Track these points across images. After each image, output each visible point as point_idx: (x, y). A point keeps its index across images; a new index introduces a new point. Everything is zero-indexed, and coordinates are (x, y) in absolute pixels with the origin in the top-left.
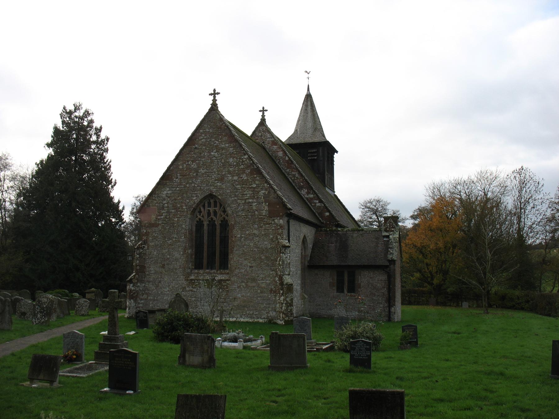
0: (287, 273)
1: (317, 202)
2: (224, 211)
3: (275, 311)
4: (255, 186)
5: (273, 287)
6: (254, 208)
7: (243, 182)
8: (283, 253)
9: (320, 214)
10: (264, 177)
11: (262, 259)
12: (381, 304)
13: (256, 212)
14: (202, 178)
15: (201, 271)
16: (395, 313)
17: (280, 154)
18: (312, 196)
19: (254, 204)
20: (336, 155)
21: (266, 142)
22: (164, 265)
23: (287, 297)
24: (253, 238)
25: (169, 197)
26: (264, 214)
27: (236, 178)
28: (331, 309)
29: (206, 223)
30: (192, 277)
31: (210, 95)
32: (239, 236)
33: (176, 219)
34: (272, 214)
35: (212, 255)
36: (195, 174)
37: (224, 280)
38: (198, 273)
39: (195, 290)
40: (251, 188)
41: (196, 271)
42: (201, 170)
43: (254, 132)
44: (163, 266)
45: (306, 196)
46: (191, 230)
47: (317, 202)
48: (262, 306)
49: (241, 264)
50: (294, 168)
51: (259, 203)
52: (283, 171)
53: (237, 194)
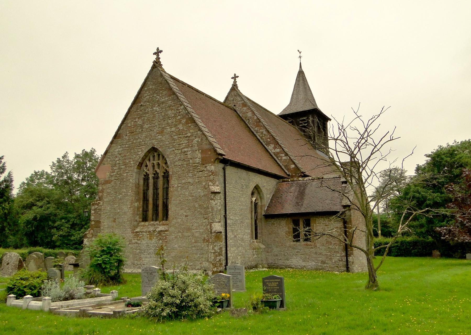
0: (217, 220)
1: (283, 155)
2: (166, 163)
3: (208, 261)
4: (189, 135)
5: (205, 236)
6: (189, 157)
7: (179, 133)
8: (212, 199)
9: (286, 166)
10: (197, 125)
11: (196, 208)
12: (338, 253)
13: (191, 161)
14: (146, 133)
15: (147, 223)
16: (353, 262)
17: (250, 114)
18: (278, 150)
19: (189, 153)
20: (329, 124)
21: (237, 106)
22: (115, 219)
23: (215, 246)
24: (188, 187)
25: (120, 154)
26: (197, 162)
27: (173, 129)
28: (287, 259)
29: (151, 176)
30: (138, 230)
31: (154, 54)
32: (176, 186)
33: (125, 175)
34: (204, 162)
35: (156, 206)
36: (140, 130)
37: (163, 231)
38: (144, 226)
39: (139, 242)
40: (186, 137)
41: (143, 223)
42: (146, 126)
43: (227, 98)
44: (114, 221)
45: (273, 151)
46: (138, 184)
47: (283, 155)
48: (196, 257)
49: (178, 214)
50: (261, 126)
51: (193, 151)
52: (252, 130)
53: (174, 144)
